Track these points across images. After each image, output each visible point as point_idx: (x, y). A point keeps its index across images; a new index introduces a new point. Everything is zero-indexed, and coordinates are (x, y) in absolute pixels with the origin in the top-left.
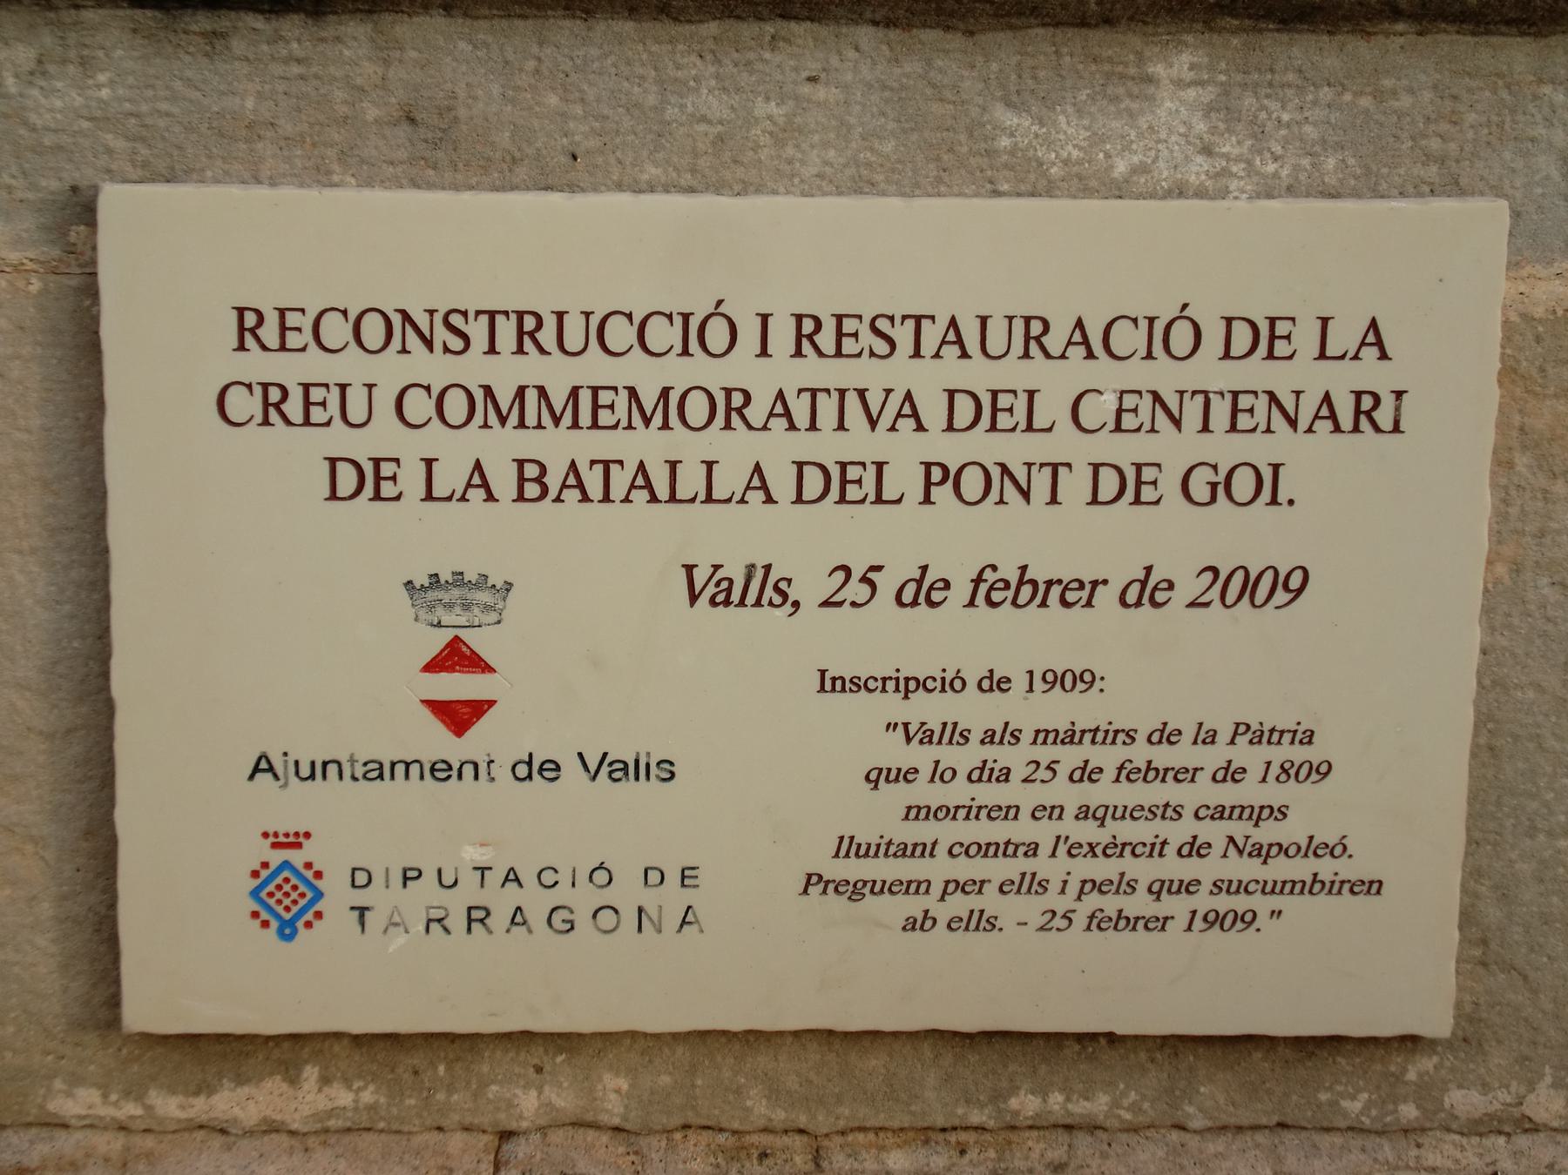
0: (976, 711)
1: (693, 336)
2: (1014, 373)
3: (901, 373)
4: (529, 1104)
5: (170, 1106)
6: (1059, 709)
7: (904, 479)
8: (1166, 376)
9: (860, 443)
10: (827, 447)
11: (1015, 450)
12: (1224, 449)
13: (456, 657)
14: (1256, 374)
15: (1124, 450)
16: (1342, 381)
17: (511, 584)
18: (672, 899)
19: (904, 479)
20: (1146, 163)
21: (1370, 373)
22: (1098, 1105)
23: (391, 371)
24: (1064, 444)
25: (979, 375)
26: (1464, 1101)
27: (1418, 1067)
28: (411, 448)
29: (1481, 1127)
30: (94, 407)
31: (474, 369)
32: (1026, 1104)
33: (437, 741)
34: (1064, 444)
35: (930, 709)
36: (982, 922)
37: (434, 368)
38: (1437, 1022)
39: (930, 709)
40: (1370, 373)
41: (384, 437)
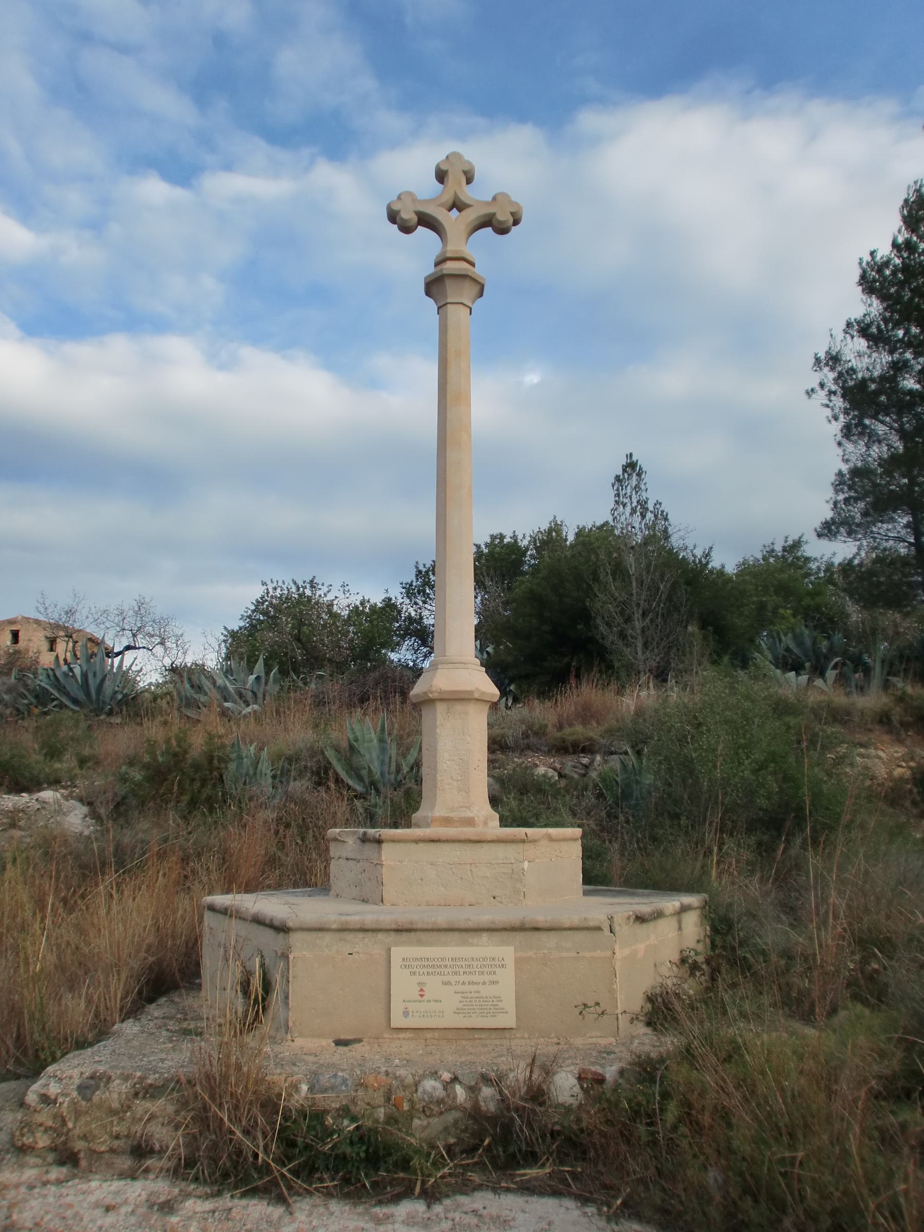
0: (468, 995)
1: (442, 960)
2: (471, 963)
3: (461, 963)
4: (428, 1036)
5: (395, 1036)
6: (477, 995)
7: (462, 973)
8: (485, 963)
9: (457, 970)
10: (454, 970)
11: (472, 970)
12: (490, 970)
13: (421, 990)
14: (493, 963)
15: (481, 970)
16: (500, 963)
17: (807, 393)
18: (441, 1014)
19: (462, 973)
20: (811, 667)
21: (503, 962)
22: (483, 1036)
23: (416, 963)
24: (476, 969)
25: (467, 963)
26: (518, 1035)
27: (514, 1032)
28: (417, 971)
29: (520, 1038)
30: (390, 967)
31: (423, 963)
32: (476, 1036)
33: (420, 998)
34: (476, 969)
35: (464, 995)
36: (470, 1016)
37: (420, 963)
38: (513, 1025)
39: (464, 995)
40: (503, 962)
41: (415, 969)
